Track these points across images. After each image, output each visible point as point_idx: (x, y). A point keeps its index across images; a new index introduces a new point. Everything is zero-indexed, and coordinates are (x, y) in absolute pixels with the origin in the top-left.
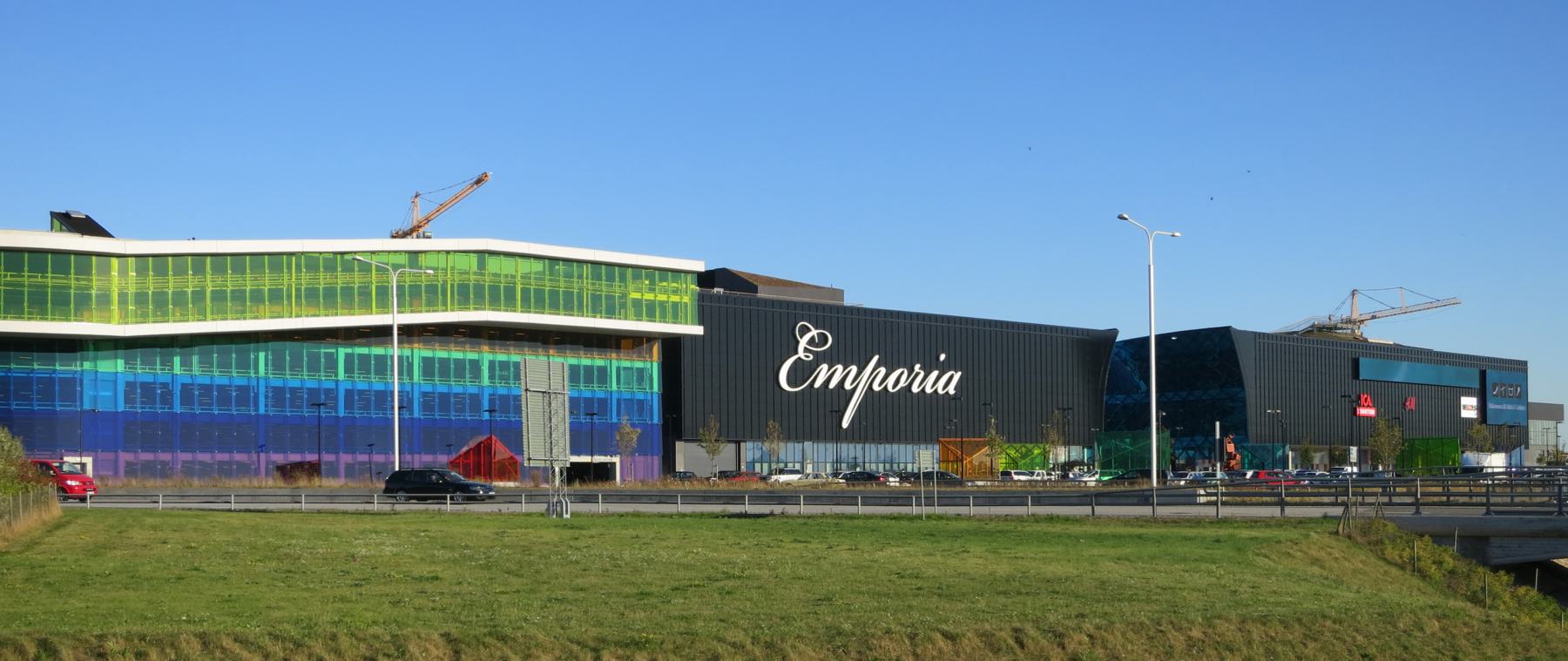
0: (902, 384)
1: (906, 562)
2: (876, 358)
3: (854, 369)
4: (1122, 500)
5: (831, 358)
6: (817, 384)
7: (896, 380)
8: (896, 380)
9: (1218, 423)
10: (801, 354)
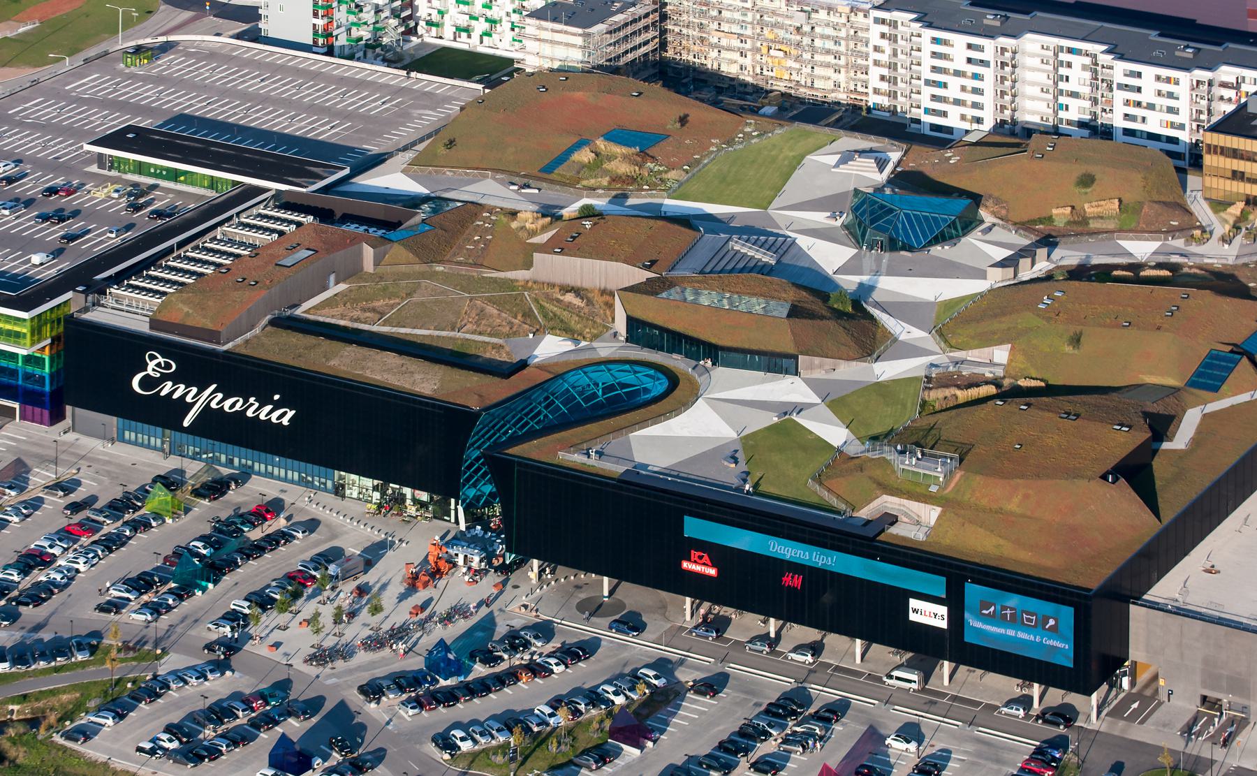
0: (237, 407)
3: (194, 390)
6: (163, 393)
8: (231, 405)
9: (712, 572)
10: (150, 371)
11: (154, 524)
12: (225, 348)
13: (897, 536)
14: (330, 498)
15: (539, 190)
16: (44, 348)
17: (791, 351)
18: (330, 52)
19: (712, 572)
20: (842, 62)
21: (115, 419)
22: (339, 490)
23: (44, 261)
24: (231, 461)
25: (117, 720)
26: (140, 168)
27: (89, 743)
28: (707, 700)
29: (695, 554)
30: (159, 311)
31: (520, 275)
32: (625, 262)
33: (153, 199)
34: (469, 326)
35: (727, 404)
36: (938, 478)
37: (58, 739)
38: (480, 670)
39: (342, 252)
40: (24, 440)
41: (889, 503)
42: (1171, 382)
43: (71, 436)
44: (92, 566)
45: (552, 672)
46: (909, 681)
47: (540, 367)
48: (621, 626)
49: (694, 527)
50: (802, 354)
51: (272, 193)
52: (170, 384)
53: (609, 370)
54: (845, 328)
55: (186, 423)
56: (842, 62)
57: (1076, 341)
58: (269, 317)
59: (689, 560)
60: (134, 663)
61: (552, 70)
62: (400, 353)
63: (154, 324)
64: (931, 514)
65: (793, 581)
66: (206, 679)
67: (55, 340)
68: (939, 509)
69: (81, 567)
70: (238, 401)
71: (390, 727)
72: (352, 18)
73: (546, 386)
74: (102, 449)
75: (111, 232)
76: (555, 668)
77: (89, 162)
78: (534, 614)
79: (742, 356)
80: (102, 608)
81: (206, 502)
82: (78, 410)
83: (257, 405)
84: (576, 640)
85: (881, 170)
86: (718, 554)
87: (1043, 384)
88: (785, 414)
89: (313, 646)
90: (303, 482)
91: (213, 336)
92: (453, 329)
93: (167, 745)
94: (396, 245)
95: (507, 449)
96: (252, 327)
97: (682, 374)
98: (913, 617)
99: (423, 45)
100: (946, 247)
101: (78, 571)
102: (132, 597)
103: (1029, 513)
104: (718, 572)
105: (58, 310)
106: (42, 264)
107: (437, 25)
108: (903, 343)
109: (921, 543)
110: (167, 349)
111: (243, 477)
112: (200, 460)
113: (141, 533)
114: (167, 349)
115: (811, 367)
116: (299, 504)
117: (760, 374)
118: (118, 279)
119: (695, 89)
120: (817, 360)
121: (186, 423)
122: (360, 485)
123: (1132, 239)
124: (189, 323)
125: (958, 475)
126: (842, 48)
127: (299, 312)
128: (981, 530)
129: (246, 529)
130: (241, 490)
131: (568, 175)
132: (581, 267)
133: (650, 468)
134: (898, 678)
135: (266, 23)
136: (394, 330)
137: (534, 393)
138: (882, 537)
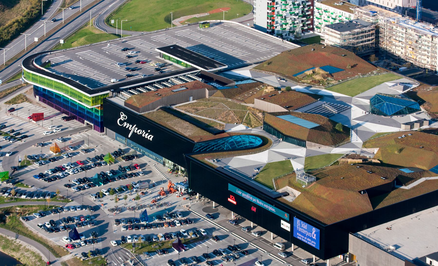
0: (140, 133)
1: (130, 197)
2: (135, 125)
3: (131, 126)
4: (175, 73)
5: (127, 121)
6: (124, 126)
7: (139, 132)
8: (139, 132)
9: (235, 203)
10: (121, 118)
11: (103, 165)
12: (141, 114)
13: (286, 201)
14: (161, 166)
15: (286, 81)
16: (98, 107)
17: (305, 138)
18: (272, 33)
19: (235, 203)
20: (430, 54)
21: (114, 133)
22: (164, 164)
23: (115, 81)
24: (140, 150)
25: (40, 216)
26: (169, 59)
27: (28, 222)
28: (215, 241)
29: (231, 196)
30: (128, 100)
31: (251, 105)
32: (281, 105)
33: (167, 68)
34: (220, 118)
35: (273, 152)
36: (306, 183)
37: (21, 219)
38: (157, 221)
39: (196, 90)
41: (288, 189)
42: (425, 168)
43: (105, 136)
44: (74, 173)
45: (176, 225)
46: (279, 247)
47: (228, 133)
48: (209, 216)
49: (231, 187)
50: (308, 141)
51: (200, 70)
52: (126, 123)
53: (249, 137)
54: (332, 135)
55: (129, 136)
56: (430, 54)
57: (401, 150)
58: (161, 106)
59: (230, 198)
60: (61, 202)
61: (331, 45)
62: (190, 123)
63: (126, 104)
64: (297, 193)
65: (254, 209)
66: (76, 210)
67: (101, 105)
68: (300, 193)
69: (70, 173)
71: (114, 232)
72: (283, 22)
73: (224, 139)
74: (109, 141)
75: (142, 76)
76: (177, 224)
77: (157, 55)
78: (188, 208)
79: (294, 140)
80: (66, 186)
81: (124, 161)
82: (107, 129)
83: (145, 133)
84: (193, 218)
85: (404, 90)
86: (237, 198)
87: (379, 162)
88: (289, 158)
89: (115, 206)
90: (157, 160)
91: (137, 109)
92: (213, 118)
93: (47, 225)
94: (219, 91)
95: (193, 155)
96: (154, 109)
97: (270, 142)
98: (282, 226)
99: (314, 34)
100: (399, 117)
101: (69, 174)
102: (77, 184)
103: (328, 199)
104: (237, 203)
105: (104, 96)
106: (114, 82)
107: (319, 28)
108: (352, 143)
109: (289, 203)
110: (126, 112)
111: (143, 155)
112: (133, 149)
114: (126, 112)
115: (311, 146)
116: (151, 166)
117: (295, 145)
118: (126, 90)
119: (386, 59)
120: (313, 144)
121: (129, 136)
122: (170, 164)
124: (134, 105)
125: (314, 183)
126: (430, 50)
127: (174, 107)
128: (309, 201)
129: (127, 170)
130: (138, 159)
131: (300, 77)
132: (268, 105)
133: (230, 168)
134: (277, 246)
135: (255, 20)
137: (219, 140)
138: (279, 199)
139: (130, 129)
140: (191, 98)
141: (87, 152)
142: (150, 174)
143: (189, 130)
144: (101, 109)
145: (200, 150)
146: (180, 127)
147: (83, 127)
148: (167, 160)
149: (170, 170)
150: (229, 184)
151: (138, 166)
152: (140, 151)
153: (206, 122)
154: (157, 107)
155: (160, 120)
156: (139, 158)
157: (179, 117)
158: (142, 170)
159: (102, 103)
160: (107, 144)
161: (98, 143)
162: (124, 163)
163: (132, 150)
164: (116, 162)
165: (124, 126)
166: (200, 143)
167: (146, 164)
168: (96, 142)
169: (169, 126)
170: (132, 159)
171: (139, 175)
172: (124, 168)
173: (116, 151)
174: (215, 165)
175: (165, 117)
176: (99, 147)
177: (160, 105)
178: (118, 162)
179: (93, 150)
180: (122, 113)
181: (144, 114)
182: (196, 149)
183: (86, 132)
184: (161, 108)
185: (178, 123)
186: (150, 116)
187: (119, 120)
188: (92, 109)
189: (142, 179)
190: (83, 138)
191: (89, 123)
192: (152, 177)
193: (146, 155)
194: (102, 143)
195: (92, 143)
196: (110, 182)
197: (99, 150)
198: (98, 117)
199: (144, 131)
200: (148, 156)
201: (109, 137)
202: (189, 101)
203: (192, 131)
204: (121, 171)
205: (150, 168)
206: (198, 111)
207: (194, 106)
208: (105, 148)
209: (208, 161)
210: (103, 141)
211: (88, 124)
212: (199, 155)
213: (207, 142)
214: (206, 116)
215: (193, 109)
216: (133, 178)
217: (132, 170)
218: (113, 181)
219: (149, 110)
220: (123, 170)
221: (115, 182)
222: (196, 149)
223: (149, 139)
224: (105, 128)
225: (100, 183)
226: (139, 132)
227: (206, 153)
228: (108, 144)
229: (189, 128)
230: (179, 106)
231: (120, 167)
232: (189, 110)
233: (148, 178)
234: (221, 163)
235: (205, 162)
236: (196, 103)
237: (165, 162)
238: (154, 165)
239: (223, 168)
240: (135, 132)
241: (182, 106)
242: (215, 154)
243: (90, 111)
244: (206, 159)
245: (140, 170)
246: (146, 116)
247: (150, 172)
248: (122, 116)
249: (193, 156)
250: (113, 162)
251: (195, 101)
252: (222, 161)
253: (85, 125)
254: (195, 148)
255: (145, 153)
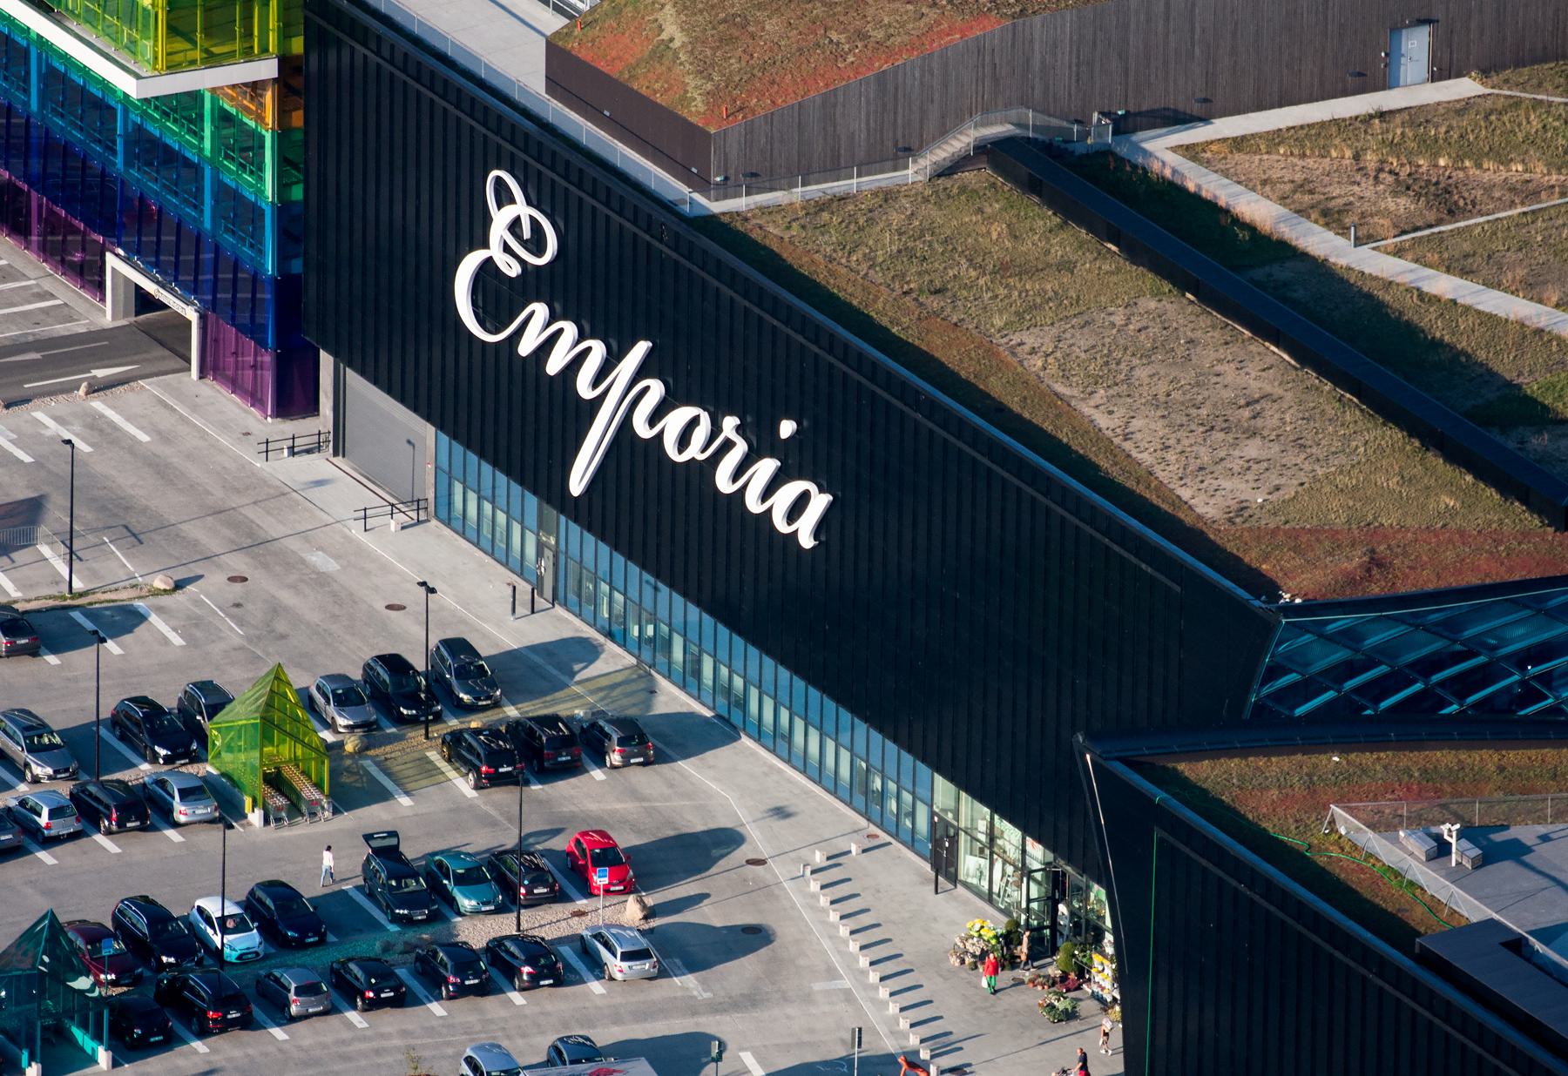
0: (694, 451)
3: (598, 349)
6: (526, 347)
11: (181, 811)
12: (717, 207)
16: (255, 88)
40: (132, 446)
43: (321, 465)
67: (287, 63)
70: (694, 422)
81: (464, 785)
83: (741, 448)
90: (863, 797)
96: (904, 152)
113: (109, 833)
116: (779, 870)
123: (522, 90)
130: (648, 780)
136: (1443, 285)
139: (585, 390)
140: (1416, 45)
141: (33, 652)
142: (740, 972)
143: (1253, 449)
144: (282, 112)
145: (1426, 704)
146: (1155, 402)
147: (79, 327)
148: (974, 815)
149: (993, 925)
150: (287, 1037)
151: (608, 856)
152: (697, 673)
153: (1505, 366)
154: (943, 132)
155: (934, 303)
156: (661, 758)
157: (1183, 282)
158: (650, 913)
159: (297, 46)
160: (318, 559)
161: (213, 544)
162: (460, 808)
163: (614, 660)
164: (345, 798)
165: (526, 347)
166: (1342, 621)
167: (728, 839)
168: (193, 531)
169: (1023, 381)
170: (572, 769)
171: (597, 968)
172: (435, 872)
173: (395, 663)
174: (1434, 905)
175: (1003, 269)
176: (210, 590)
177: (986, 110)
178: (383, 796)
179: (126, 620)
180: (500, 183)
181: (764, 210)
182: (1306, 689)
183: (97, 404)
184: (992, 153)
185: (1147, 356)
186: (827, 242)
187: (470, 263)
188: (185, 107)
189: (617, 1020)
190: (38, 464)
191: (150, 287)
192: (749, 1001)
193: (759, 737)
194: (256, 545)
195: (134, 537)
196: (203, 1034)
197: (193, 625)
198: (236, 208)
199: (730, 423)
200: (778, 741)
201: (373, 476)
202: (1383, 80)
203: (1292, 458)
204: (387, 909)
205: (768, 890)
206: (1453, 213)
207: (1431, 147)
208: (276, 609)
209: (1373, 841)
210: (271, 527)
211: (145, 302)
212: (1277, 766)
213: (1435, 614)
214: (1531, 288)
215: (1403, 187)
216: (517, 998)
217: (535, 903)
218: (247, 1023)
219: (835, 170)
220: (412, 901)
221: (278, 1033)
222: (1306, 689)
223: (782, 526)
224: (326, 361)
225: (78, 1033)
226: (684, 441)
227: (1375, 742)
228: (331, 566)
229: (1270, 420)
230: (1239, 143)
231: (377, 852)
232: (1339, 192)
233: (692, 1007)
234: (1530, 881)
235: (1329, 858)
236: (1463, 107)
237: (954, 840)
238: (819, 858)
239: (1517, 945)
240: (643, 431)
241: (1275, 138)
242: (1485, 759)
243: (173, 134)
244: (1346, 822)
245: (631, 912)
246: (774, 234)
247: (753, 937)
248: (500, 220)
249: (1205, 772)
250: (309, 792)
251: (1466, 87)
252: (1543, 855)
253: (107, 315)
254: (1274, 672)
255: (743, 704)
